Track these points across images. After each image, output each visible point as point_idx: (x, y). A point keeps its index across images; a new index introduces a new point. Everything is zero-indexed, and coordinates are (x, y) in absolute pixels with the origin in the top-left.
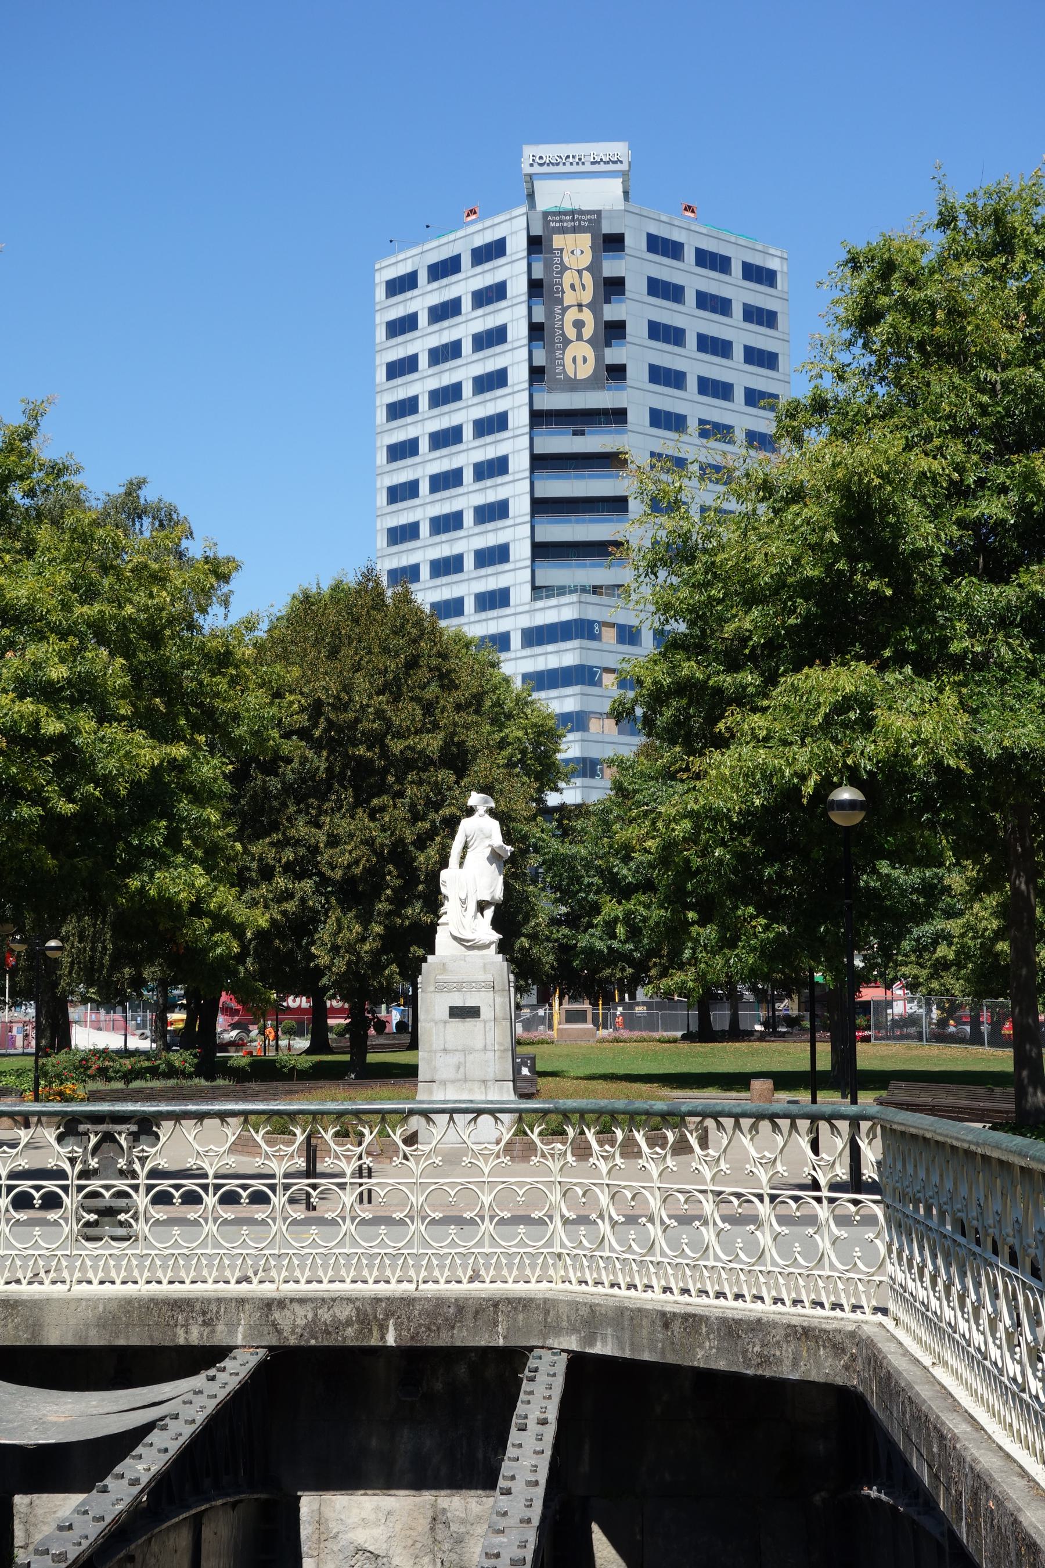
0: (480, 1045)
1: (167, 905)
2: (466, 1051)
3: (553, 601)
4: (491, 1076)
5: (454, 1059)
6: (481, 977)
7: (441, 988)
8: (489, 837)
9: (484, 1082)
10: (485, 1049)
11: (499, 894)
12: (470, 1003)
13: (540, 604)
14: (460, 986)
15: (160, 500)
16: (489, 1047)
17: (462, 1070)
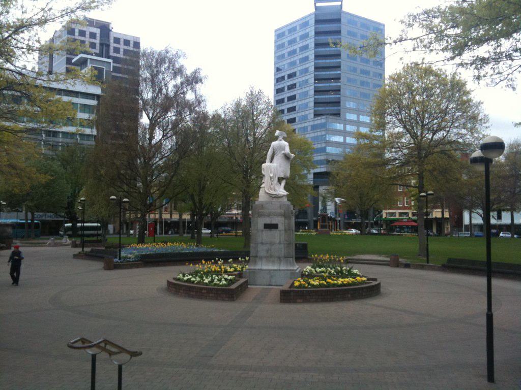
0: (278, 241)
1: (115, 130)
2: (272, 244)
3: (319, 118)
4: (282, 255)
5: (265, 247)
6: (279, 211)
7: (260, 215)
8: (284, 150)
9: (279, 258)
10: (280, 243)
11: (288, 175)
12: (274, 222)
13: (316, 119)
14: (269, 215)
15: (167, 52)
16: (282, 242)
17: (269, 252)
